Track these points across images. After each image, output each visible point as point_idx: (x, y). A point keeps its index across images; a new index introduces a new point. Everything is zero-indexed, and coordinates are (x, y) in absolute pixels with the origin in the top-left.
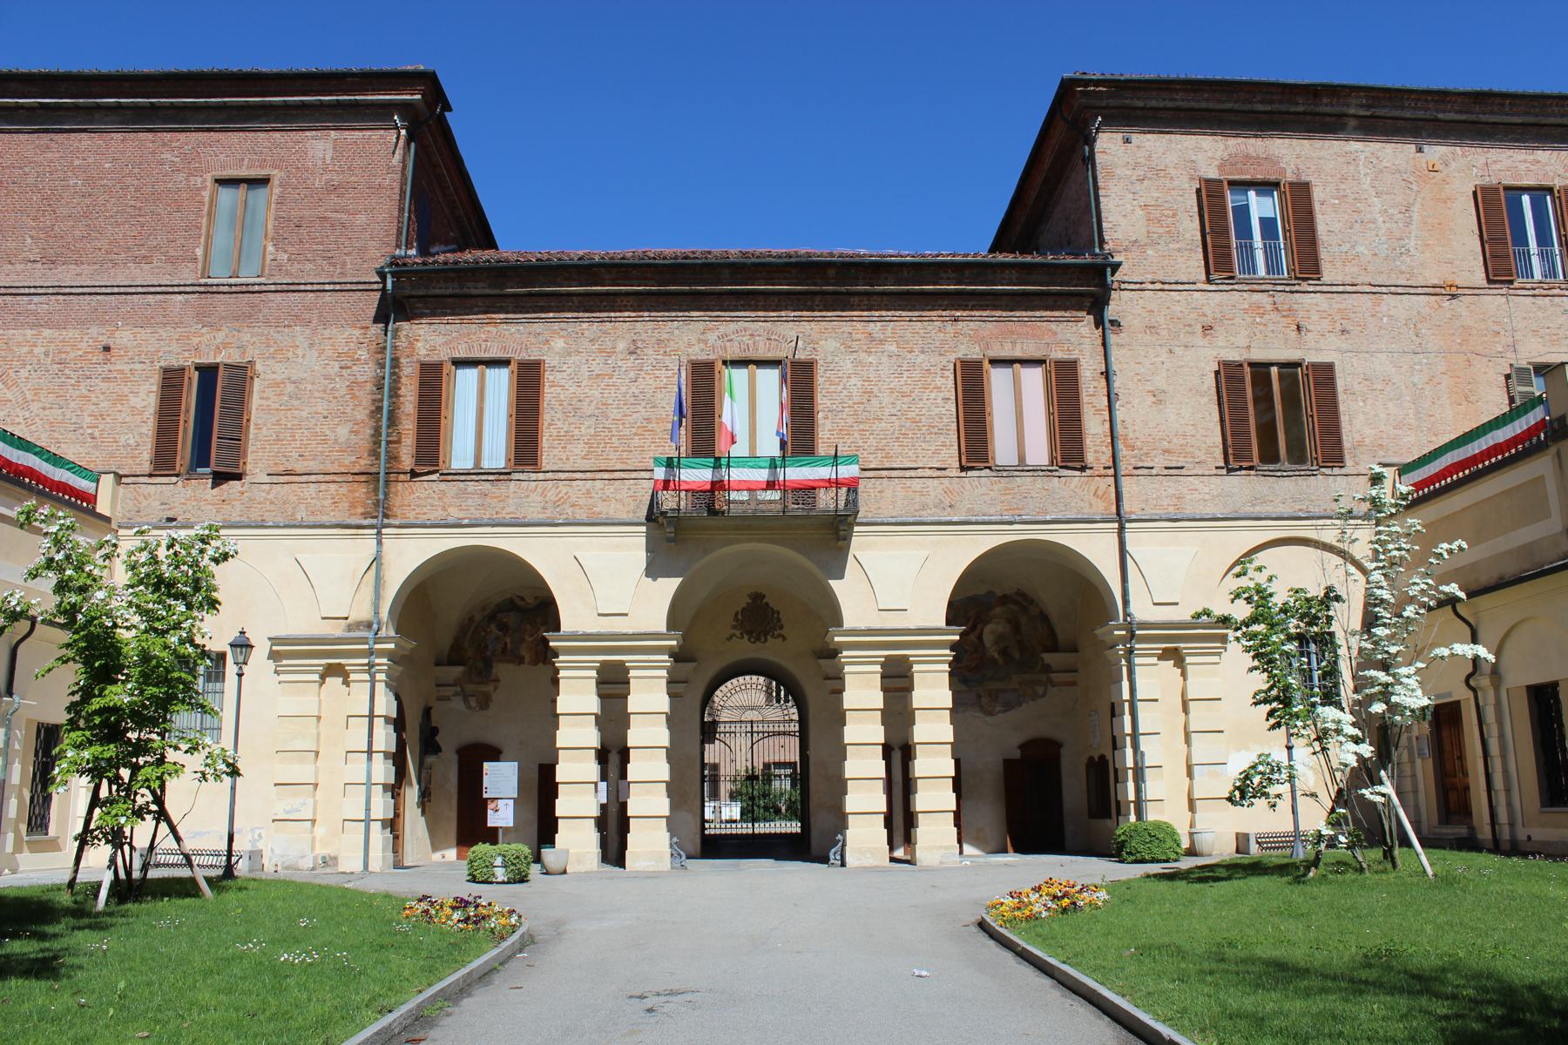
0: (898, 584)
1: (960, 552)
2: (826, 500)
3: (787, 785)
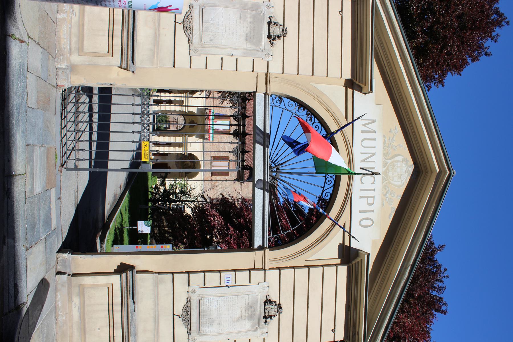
0: (194, 146)
1: (199, 156)
2: (207, 136)
3: (165, 126)
